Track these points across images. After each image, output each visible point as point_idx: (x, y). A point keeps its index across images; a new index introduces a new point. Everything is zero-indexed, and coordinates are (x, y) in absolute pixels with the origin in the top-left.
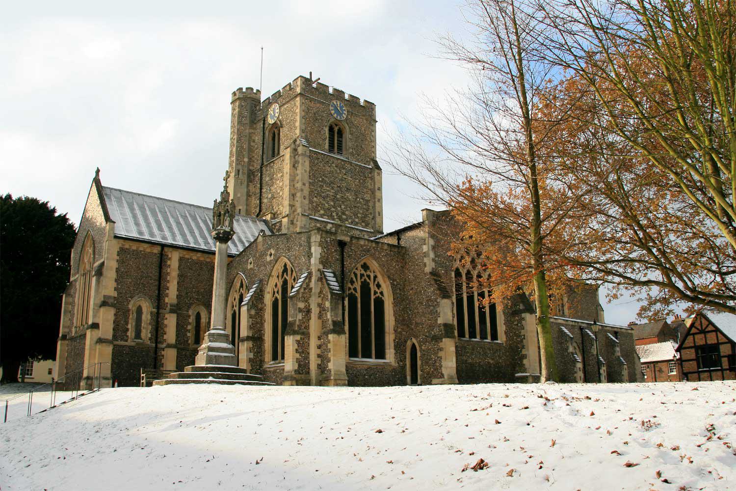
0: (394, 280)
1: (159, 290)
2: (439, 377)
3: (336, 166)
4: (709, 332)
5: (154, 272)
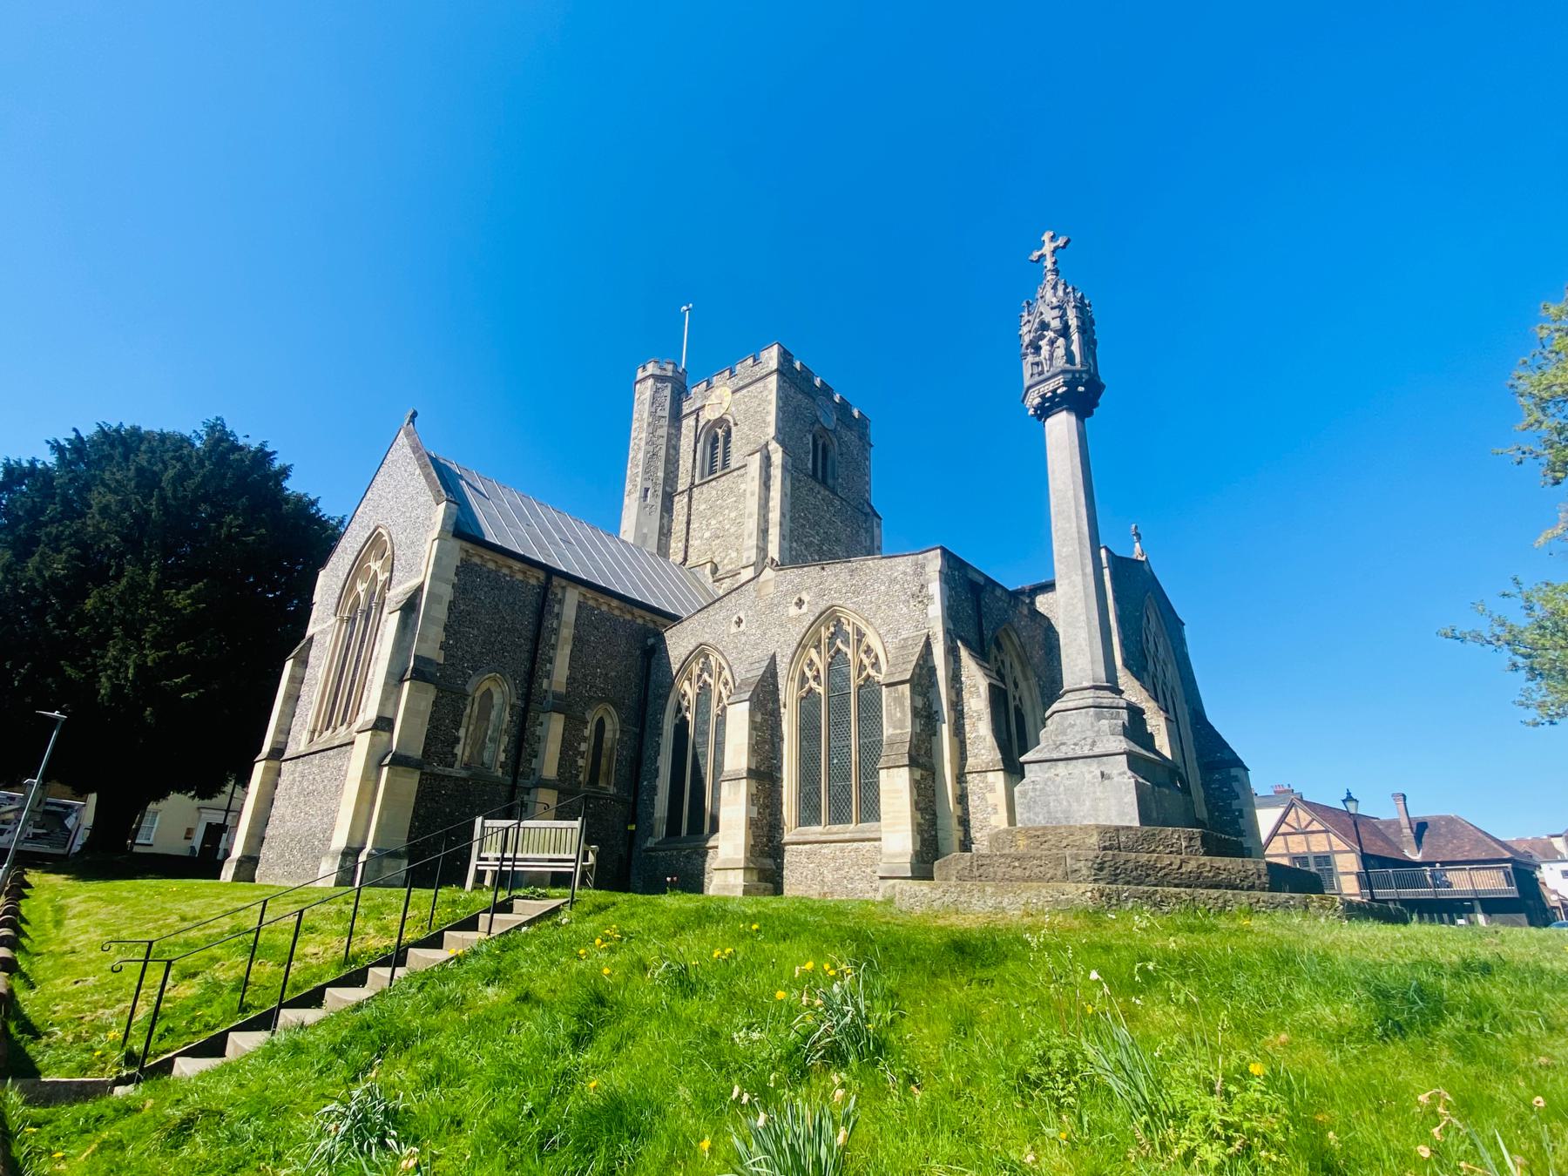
0: (1040, 678)
1: (533, 660)
4: (1313, 832)
5: (526, 621)
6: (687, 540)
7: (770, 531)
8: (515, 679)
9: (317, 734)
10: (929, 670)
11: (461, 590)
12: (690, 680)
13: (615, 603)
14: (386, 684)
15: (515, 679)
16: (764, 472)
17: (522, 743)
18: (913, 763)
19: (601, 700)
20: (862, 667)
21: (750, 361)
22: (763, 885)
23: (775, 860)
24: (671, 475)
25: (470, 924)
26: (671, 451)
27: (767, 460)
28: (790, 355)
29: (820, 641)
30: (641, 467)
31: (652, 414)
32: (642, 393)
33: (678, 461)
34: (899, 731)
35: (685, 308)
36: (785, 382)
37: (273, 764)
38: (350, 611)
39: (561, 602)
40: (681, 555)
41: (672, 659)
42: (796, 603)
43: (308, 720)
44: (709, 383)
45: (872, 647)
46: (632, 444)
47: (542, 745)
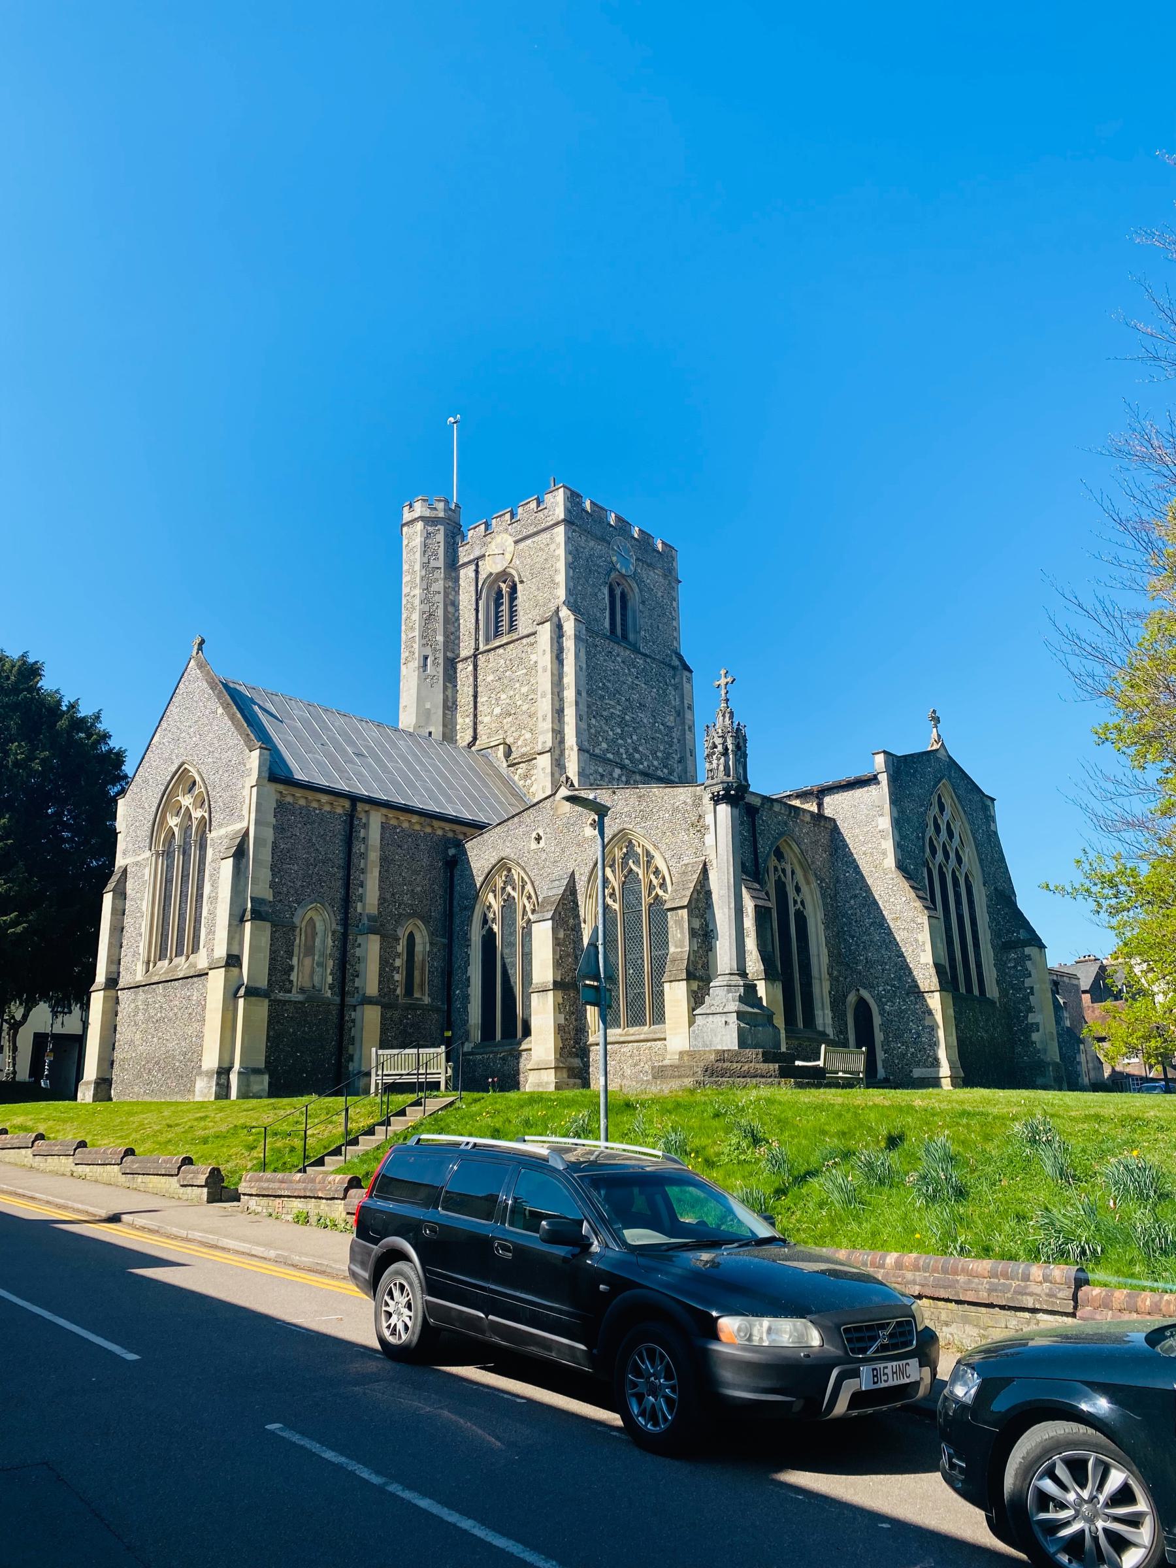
0: (822, 880)
1: (347, 885)
2: (929, 1064)
3: (623, 662)
6: (475, 716)
7: (566, 712)
8: (333, 907)
9: (151, 965)
10: (706, 893)
11: (279, 829)
12: (494, 892)
13: (415, 818)
14: (230, 925)
15: (333, 907)
16: (556, 644)
17: (345, 966)
18: (690, 976)
19: (411, 916)
20: (651, 887)
21: (533, 505)
22: (572, 1081)
23: (582, 1059)
24: (452, 637)
25: (402, 1113)
26: (451, 609)
27: (558, 629)
28: (579, 496)
29: (614, 860)
30: (417, 631)
31: (425, 565)
32: (410, 539)
33: (458, 619)
34: (679, 950)
35: (452, 419)
36: (574, 531)
37: (112, 993)
38: (164, 845)
39: (366, 826)
40: (470, 732)
41: (474, 872)
42: (591, 824)
43: (141, 951)
44: (487, 526)
45: (660, 868)
46: (404, 602)
47: (362, 965)
